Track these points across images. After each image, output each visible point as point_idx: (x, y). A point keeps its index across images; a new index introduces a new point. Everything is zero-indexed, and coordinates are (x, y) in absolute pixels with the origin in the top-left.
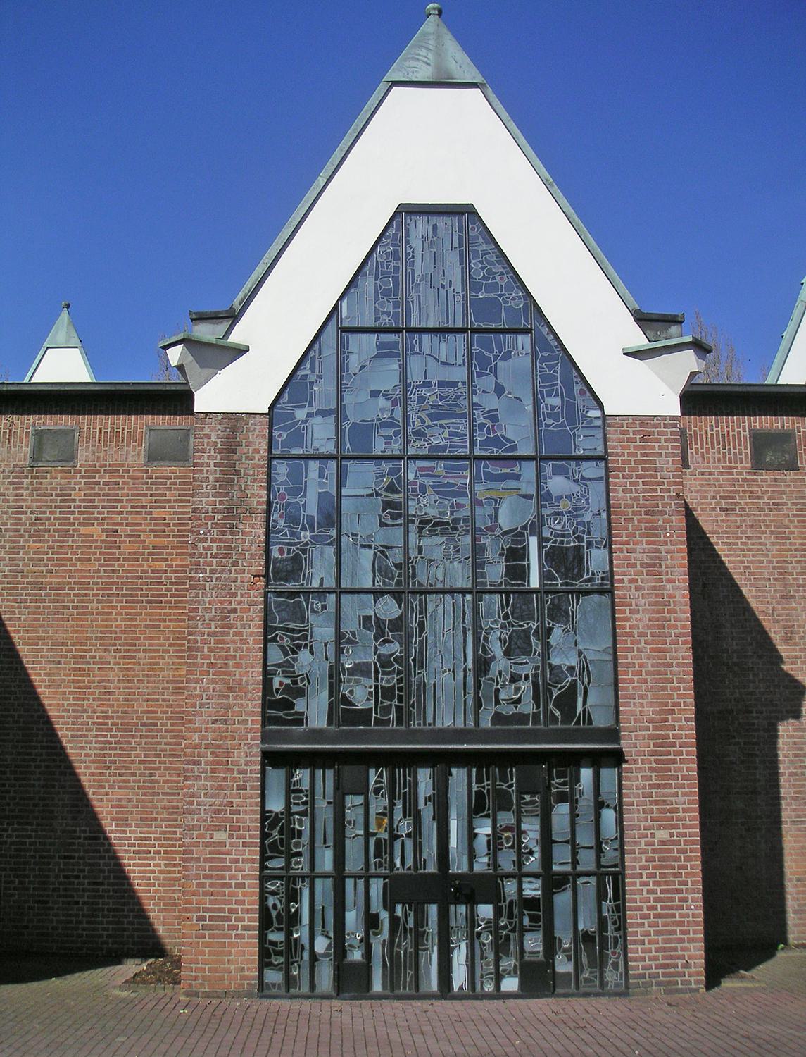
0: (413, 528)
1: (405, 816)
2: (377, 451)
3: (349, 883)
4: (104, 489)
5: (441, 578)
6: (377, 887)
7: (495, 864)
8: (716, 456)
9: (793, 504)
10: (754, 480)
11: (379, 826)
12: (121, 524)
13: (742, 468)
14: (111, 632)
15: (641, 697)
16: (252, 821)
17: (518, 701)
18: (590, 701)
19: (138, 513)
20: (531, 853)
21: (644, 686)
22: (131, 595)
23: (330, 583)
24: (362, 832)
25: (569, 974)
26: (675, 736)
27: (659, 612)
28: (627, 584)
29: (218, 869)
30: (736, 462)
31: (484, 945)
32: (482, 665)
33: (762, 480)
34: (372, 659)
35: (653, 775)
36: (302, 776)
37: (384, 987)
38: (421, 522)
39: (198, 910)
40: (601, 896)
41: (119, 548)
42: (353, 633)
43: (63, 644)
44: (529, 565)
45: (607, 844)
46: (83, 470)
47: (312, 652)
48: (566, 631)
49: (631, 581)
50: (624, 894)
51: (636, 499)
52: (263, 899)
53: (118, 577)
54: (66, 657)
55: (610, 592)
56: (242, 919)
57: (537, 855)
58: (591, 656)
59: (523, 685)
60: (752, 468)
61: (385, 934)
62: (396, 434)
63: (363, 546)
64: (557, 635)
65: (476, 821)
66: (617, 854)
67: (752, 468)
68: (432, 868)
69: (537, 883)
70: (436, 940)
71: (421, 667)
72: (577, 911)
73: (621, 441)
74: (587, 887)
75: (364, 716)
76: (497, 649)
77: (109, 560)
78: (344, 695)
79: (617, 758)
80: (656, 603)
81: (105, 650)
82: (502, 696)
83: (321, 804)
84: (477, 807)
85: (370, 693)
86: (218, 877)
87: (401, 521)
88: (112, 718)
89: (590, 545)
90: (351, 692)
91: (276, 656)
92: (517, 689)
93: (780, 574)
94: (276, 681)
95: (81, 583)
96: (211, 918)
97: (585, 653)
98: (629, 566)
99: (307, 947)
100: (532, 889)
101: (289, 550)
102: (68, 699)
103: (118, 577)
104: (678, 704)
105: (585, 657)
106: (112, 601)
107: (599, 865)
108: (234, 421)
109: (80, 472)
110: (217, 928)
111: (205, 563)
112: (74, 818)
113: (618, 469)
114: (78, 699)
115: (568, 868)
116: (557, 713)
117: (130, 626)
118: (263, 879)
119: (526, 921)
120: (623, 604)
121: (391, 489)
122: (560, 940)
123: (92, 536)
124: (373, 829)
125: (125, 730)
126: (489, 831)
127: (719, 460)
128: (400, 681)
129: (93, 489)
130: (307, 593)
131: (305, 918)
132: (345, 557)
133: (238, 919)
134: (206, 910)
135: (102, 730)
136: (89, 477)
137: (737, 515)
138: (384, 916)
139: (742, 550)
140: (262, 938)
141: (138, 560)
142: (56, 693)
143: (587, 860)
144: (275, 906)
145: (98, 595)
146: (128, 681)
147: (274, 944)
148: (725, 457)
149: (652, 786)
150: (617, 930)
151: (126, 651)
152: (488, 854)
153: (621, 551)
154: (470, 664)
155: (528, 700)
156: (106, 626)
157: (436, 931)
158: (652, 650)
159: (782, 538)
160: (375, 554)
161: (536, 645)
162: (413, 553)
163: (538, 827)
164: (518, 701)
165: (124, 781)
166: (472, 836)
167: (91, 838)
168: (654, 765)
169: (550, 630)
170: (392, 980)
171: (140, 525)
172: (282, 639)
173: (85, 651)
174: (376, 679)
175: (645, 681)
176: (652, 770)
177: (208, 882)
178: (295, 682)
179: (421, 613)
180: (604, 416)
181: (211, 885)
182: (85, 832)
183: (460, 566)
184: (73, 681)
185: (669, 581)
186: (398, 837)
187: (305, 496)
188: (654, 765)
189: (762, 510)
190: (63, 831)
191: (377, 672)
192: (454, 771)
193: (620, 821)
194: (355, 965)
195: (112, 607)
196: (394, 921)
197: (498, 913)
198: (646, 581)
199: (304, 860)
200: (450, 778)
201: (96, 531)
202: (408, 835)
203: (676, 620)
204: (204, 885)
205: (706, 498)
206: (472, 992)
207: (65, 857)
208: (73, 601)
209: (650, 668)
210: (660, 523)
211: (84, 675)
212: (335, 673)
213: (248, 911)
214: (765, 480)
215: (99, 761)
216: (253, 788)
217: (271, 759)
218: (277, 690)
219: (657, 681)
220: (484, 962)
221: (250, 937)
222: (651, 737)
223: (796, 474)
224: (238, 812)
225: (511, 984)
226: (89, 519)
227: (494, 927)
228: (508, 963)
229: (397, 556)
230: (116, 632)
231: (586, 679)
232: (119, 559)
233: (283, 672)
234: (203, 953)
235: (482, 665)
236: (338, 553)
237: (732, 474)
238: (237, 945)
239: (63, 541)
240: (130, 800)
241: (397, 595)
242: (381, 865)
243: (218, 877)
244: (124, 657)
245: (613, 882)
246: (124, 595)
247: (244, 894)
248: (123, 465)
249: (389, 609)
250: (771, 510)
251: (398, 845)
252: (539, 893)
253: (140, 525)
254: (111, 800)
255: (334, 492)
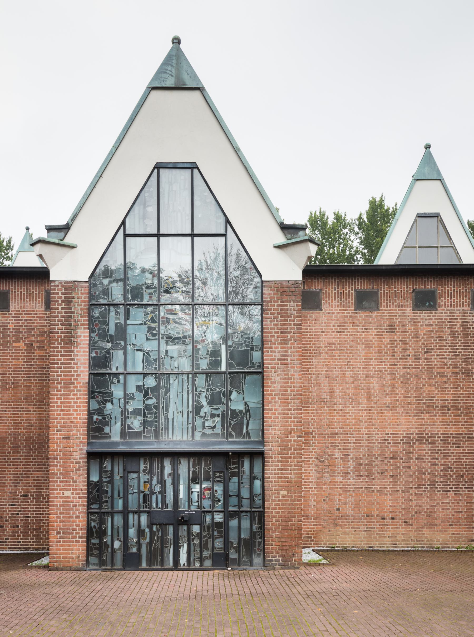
0: (163, 341)
1: (158, 483)
2: (145, 302)
3: (131, 516)
4: (24, 323)
5: (177, 366)
6: (144, 519)
8: (336, 304)
9: (375, 329)
10: (355, 317)
11: (145, 487)
12: (34, 341)
13: (350, 310)
14: (31, 396)
15: (275, 425)
16: (83, 486)
17: (214, 427)
18: (250, 428)
19: (42, 335)
20: (219, 501)
21: (277, 420)
22: (41, 377)
23: (121, 370)
24: (136, 491)
25: (236, 558)
26: (291, 445)
27: (286, 383)
28: (270, 369)
29: (67, 509)
30: (346, 307)
31: (196, 544)
32: (197, 409)
33: (360, 317)
34: (142, 406)
35: (280, 464)
36: (108, 464)
37: (147, 565)
38: (167, 338)
39: (57, 529)
41: (34, 353)
42: (133, 394)
43: (7, 402)
44: (221, 359)
45: (256, 497)
46: (13, 313)
47: (112, 404)
50: (264, 521)
51: (276, 325)
53: (34, 368)
54: (9, 408)
55: (261, 374)
56: (79, 533)
57: (222, 502)
58: (251, 405)
59: (217, 419)
60: (355, 310)
61: (148, 540)
62: (155, 292)
63: (137, 350)
64: (234, 395)
65: (192, 486)
66: (261, 502)
67: (355, 310)
68: (170, 509)
69: (221, 515)
70: (172, 542)
71: (166, 411)
73: (270, 294)
75: (138, 434)
76: (204, 402)
77: (29, 359)
78: (128, 425)
79: (261, 454)
80: (285, 379)
81: (29, 405)
82: (206, 424)
83: (117, 477)
84: (194, 479)
85: (141, 423)
86: (67, 513)
87: (157, 337)
88: (33, 437)
89: (252, 349)
90: (132, 423)
92: (214, 421)
93: (366, 365)
94: (95, 417)
95: (15, 371)
96: (63, 533)
97: (248, 403)
98: (271, 360)
99: (110, 546)
100: (219, 518)
101: (101, 352)
102: (11, 429)
103: (34, 368)
104: (294, 429)
105: (248, 406)
106: (31, 380)
107: (251, 507)
108: (71, 286)
109: (11, 314)
110: (66, 537)
111: (58, 359)
112: (16, 486)
113: (268, 310)
114: (16, 429)
115: (236, 509)
116: (233, 433)
117: (41, 392)
119: (216, 533)
120: (267, 379)
121: (152, 320)
122: (232, 543)
123: (19, 347)
124: (142, 488)
125: (40, 443)
126: (198, 490)
127: (338, 306)
128: (156, 418)
129: (19, 323)
130: (110, 374)
131: (109, 533)
132: (129, 357)
133: (77, 533)
134: (61, 529)
135: (28, 443)
136: (16, 317)
137: (345, 335)
138: (147, 530)
139: (347, 353)
140: (88, 542)
141: (43, 359)
142: (5, 426)
143: (246, 505)
144: (95, 527)
145: (24, 377)
146: (41, 420)
147: (94, 544)
148: (341, 305)
149: (279, 469)
150: (260, 538)
151: (39, 405)
152: (198, 501)
153: (268, 352)
154: (190, 409)
155: (219, 426)
156: (29, 393)
157: (172, 538)
158: (281, 402)
159: (368, 347)
160: (144, 354)
161: (223, 400)
162: (163, 354)
163: (222, 488)
164: (214, 427)
165: (40, 468)
166: (190, 492)
167: (24, 496)
168: (280, 459)
169: (231, 393)
170: (150, 562)
171: (44, 342)
172: (97, 397)
173: (19, 405)
174: (144, 417)
175: (277, 418)
176: (279, 461)
177: (62, 515)
178: (104, 419)
179: (167, 384)
180: (262, 282)
181: (63, 517)
182: (21, 492)
183: (186, 360)
184: (13, 420)
185: (292, 367)
186: (154, 493)
187: (108, 325)
188: (280, 459)
189: (358, 332)
190: (10, 493)
191: (144, 414)
192: (182, 461)
194: (132, 554)
195: (31, 383)
196: (152, 533)
197: (202, 529)
199: (109, 504)
201: (21, 345)
202: (159, 492)
203: (294, 387)
204: (60, 517)
205: (330, 326)
206: (189, 567)
207: (12, 505)
208: (11, 380)
209: (280, 411)
210: (289, 337)
211: (18, 417)
212: (124, 413)
213: (82, 529)
214: (362, 316)
215: (27, 459)
216: (83, 470)
217: (91, 456)
218: (95, 422)
220: (195, 553)
221: (82, 541)
222: (279, 445)
223: (378, 313)
224: (76, 482)
225: (208, 563)
226: (18, 339)
227: (200, 535)
228: (206, 553)
229: (154, 356)
230: (33, 396)
231: (248, 417)
232: (34, 359)
233: (98, 413)
234: (59, 550)
235: (197, 409)
236: (125, 354)
237: (344, 313)
238: (76, 545)
239: (5, 350)
240: (43, 477)
241: (156, 375)
242: (146, 507)
243: (67, 513)
244: (38, 408)
246: (37, 377)
247: (80, 521)
248: (33, 311)
249: (151, 382)
250: (363, 332)
251: (154, 497)
252: (222, 520)
253: (44, 342)
254: (34, 477)
255: (123, 323)
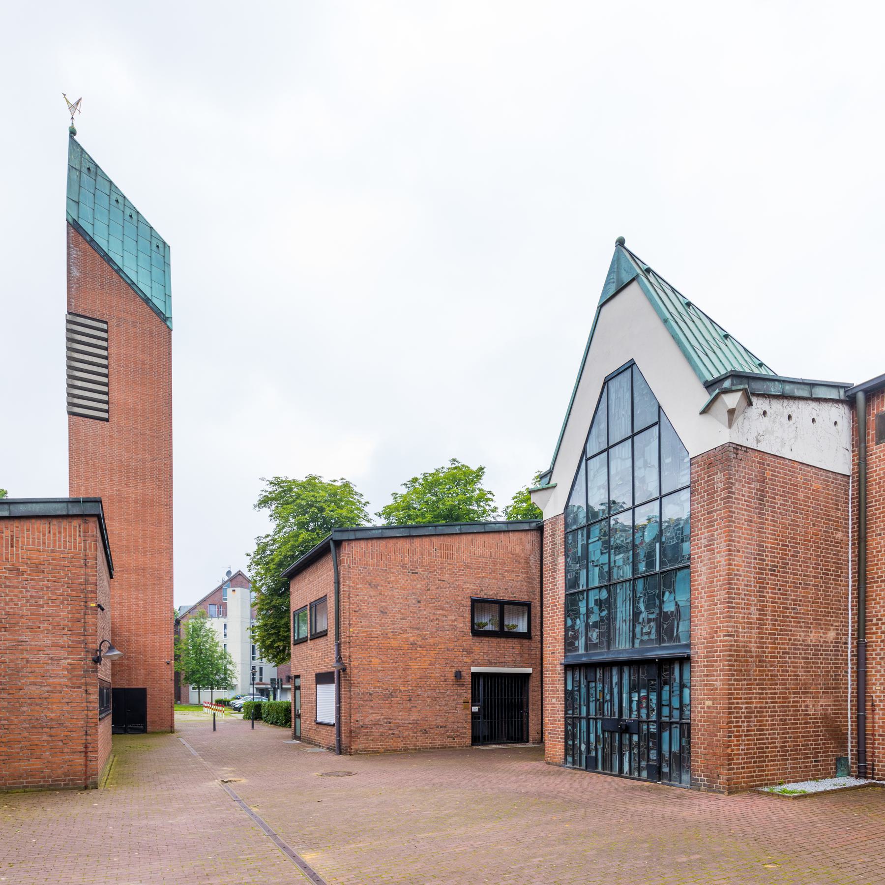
3: (591, 721)
7: (639, 715)
27: (712, 573)
40: (681, 735)
48: (670, 593)
49: (699, 557)
52: (566, 727)
59: (652, 624)
72: (670, 743)
74: (676, 732)
80: (711, 568)
83: (583, 686)
84: (633, 688)
91: (569, 623)
100: (653, 728)
107: (681, 718)
118: (566, 718)
149: (705, 676)
175: (703, 615)
193: (566, 684)
198: (706, 556)
200: (749, 637)
219: (710, 615)
222: (705, 648)
225: (644, 774)
245: (686, 729)
249: (604, 594)
